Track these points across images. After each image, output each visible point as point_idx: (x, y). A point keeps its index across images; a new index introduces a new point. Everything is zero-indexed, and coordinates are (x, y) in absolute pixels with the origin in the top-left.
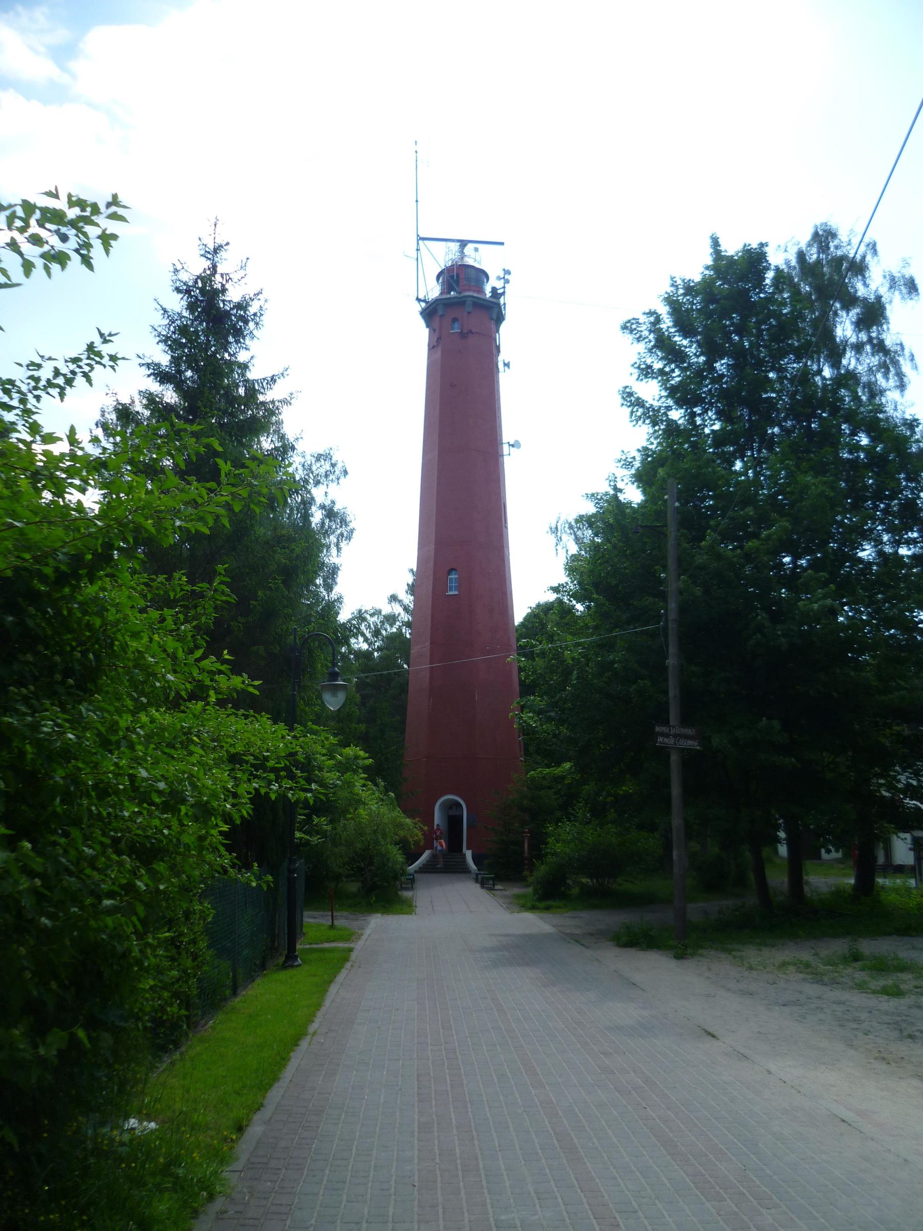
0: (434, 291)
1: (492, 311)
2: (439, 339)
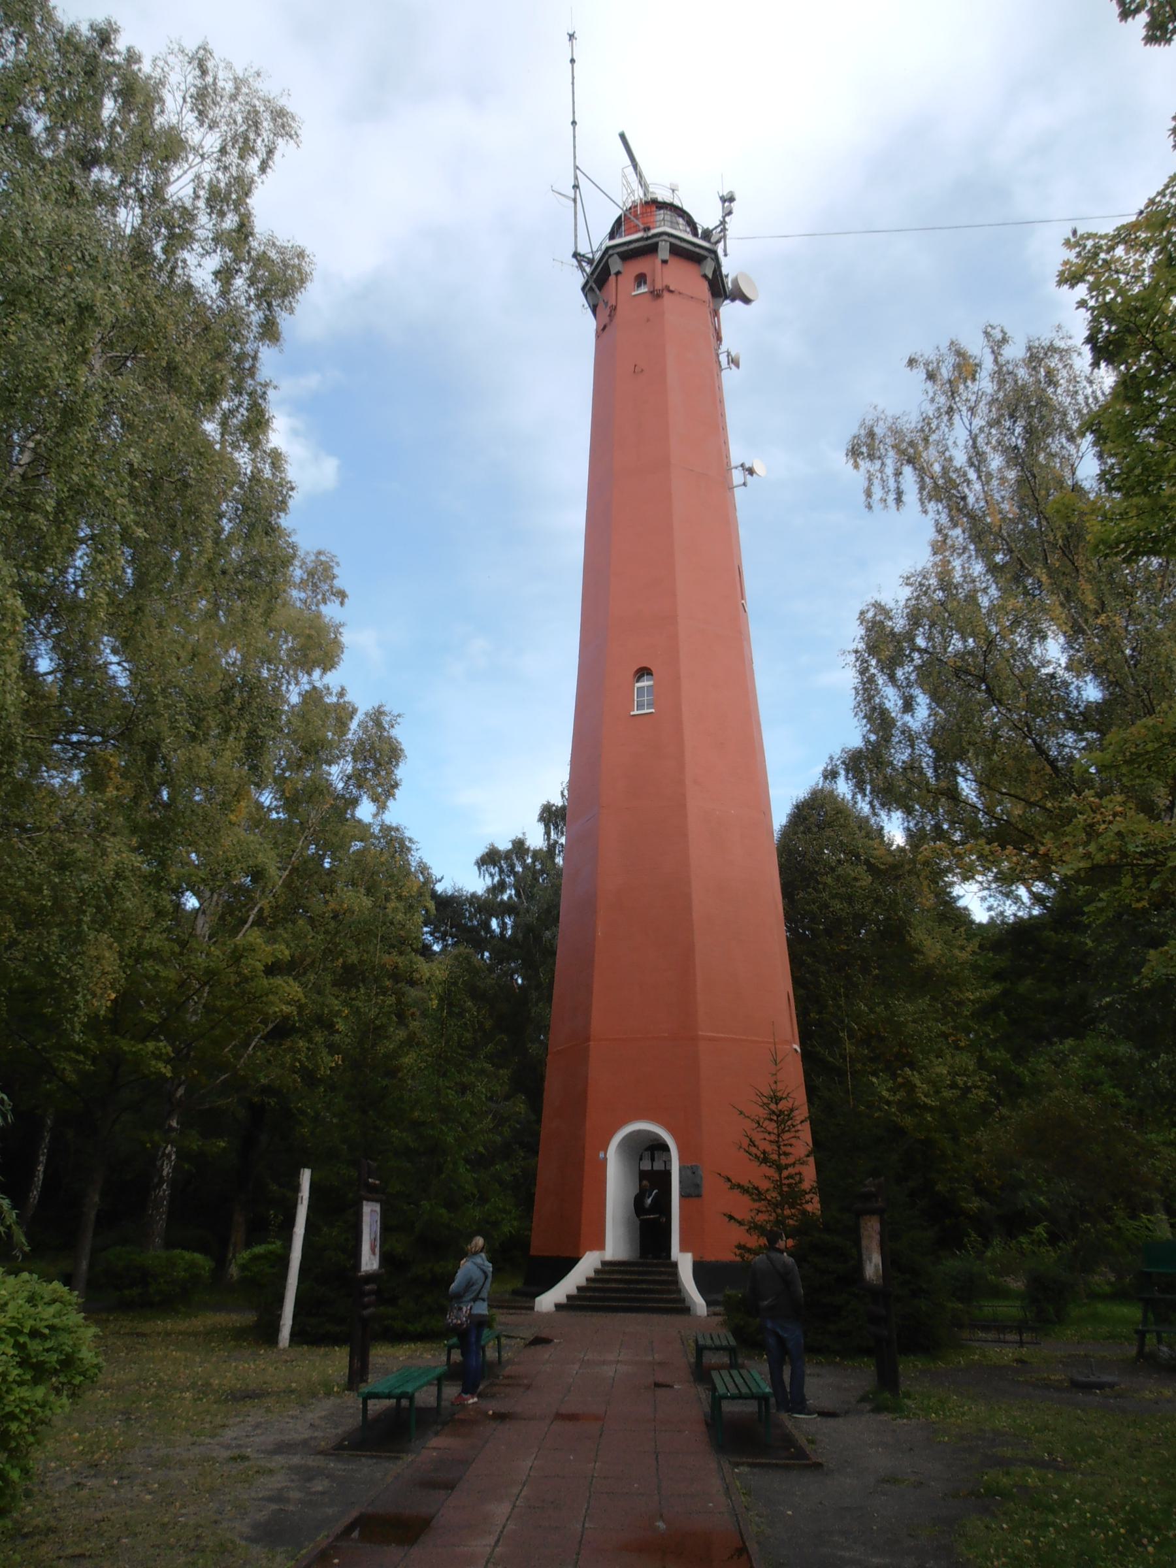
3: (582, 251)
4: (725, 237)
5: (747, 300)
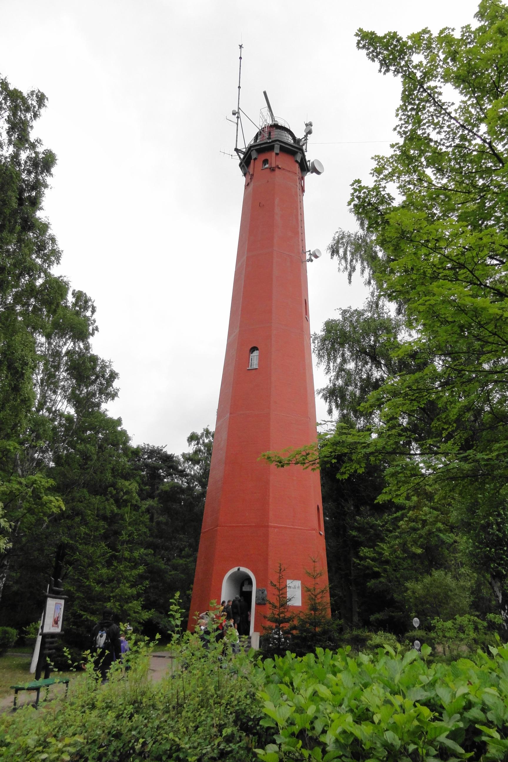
3: (239, 148)
4: (306, 143)
5: (318, 173)
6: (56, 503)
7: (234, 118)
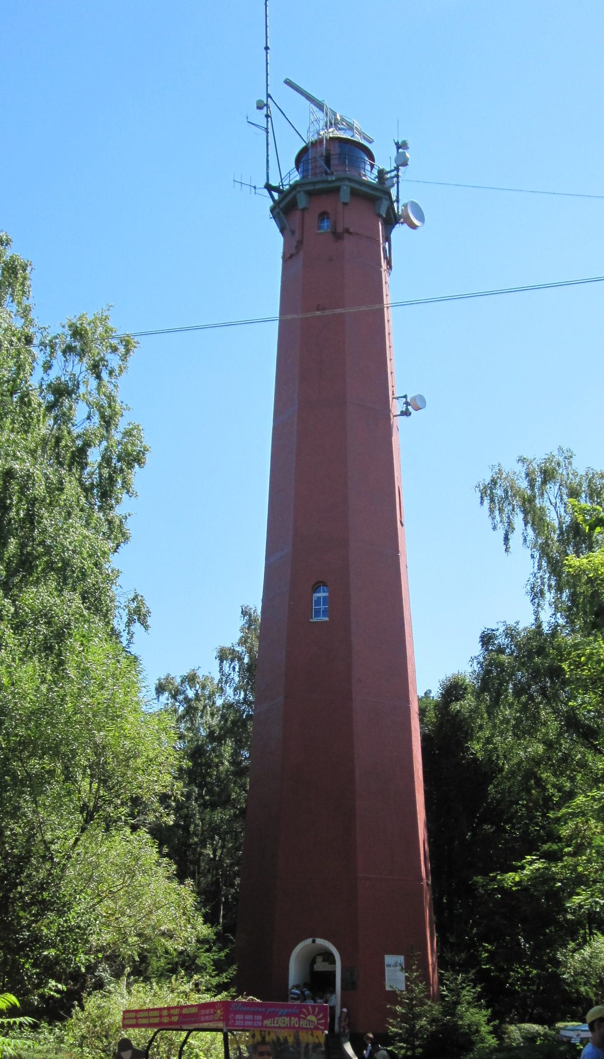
0: (287, 174)
1: (378, 206)
2: (300, 243)
6: (83, 970)
7: (259, 117)
